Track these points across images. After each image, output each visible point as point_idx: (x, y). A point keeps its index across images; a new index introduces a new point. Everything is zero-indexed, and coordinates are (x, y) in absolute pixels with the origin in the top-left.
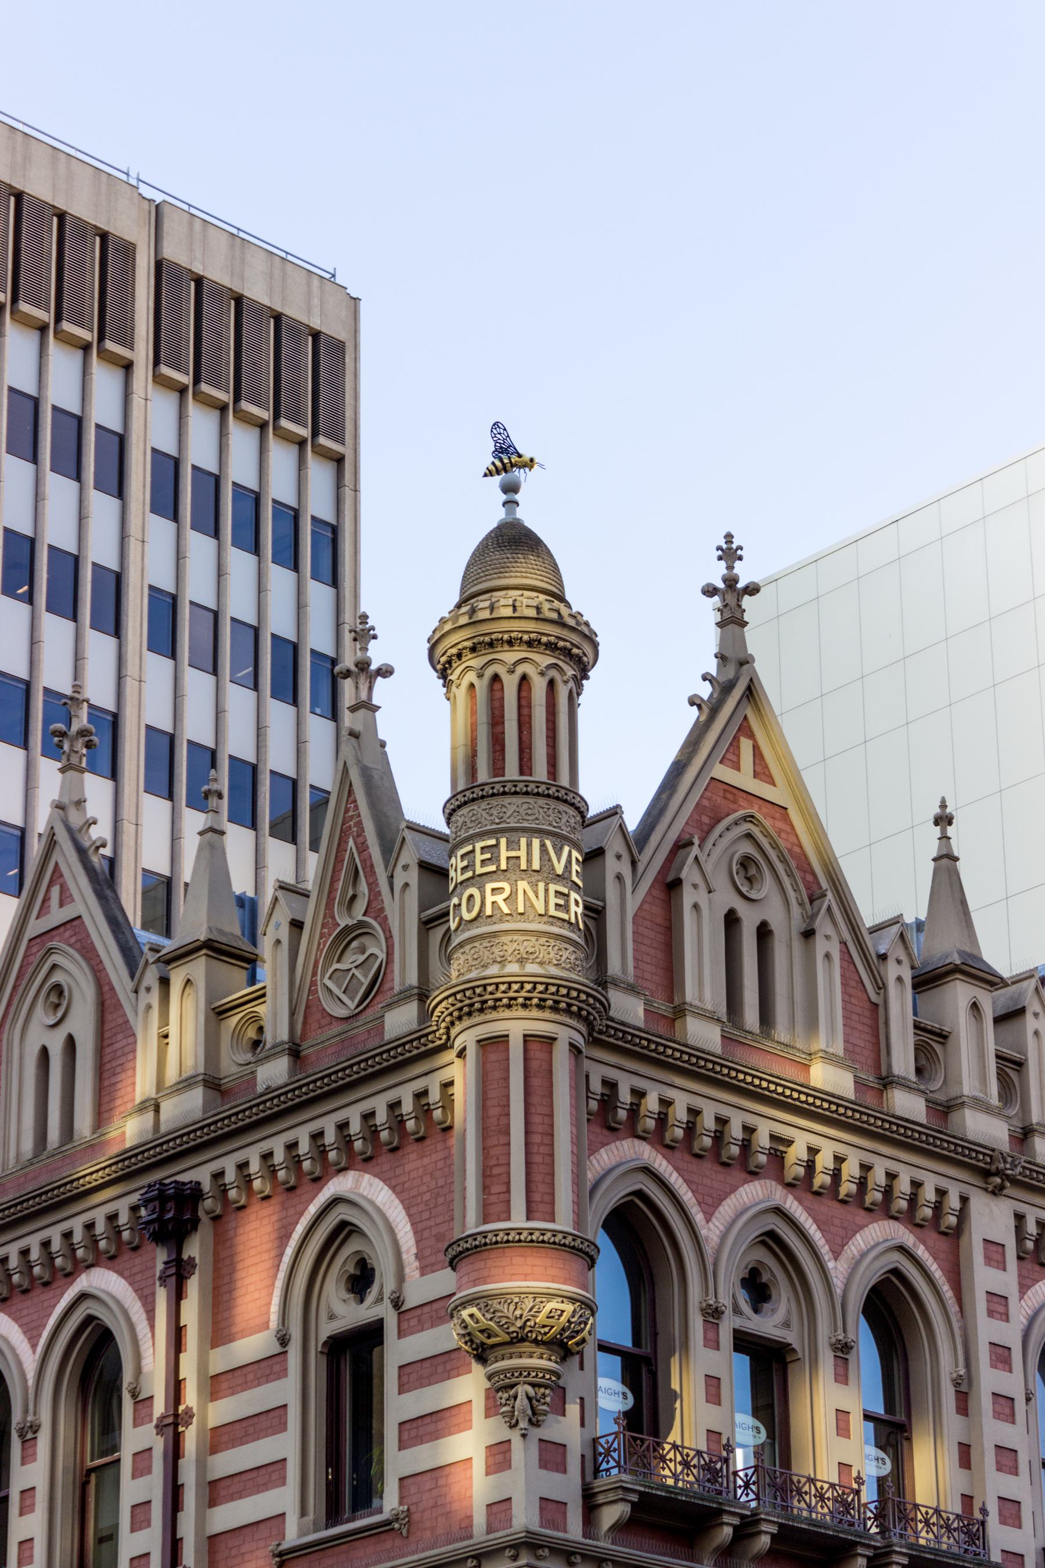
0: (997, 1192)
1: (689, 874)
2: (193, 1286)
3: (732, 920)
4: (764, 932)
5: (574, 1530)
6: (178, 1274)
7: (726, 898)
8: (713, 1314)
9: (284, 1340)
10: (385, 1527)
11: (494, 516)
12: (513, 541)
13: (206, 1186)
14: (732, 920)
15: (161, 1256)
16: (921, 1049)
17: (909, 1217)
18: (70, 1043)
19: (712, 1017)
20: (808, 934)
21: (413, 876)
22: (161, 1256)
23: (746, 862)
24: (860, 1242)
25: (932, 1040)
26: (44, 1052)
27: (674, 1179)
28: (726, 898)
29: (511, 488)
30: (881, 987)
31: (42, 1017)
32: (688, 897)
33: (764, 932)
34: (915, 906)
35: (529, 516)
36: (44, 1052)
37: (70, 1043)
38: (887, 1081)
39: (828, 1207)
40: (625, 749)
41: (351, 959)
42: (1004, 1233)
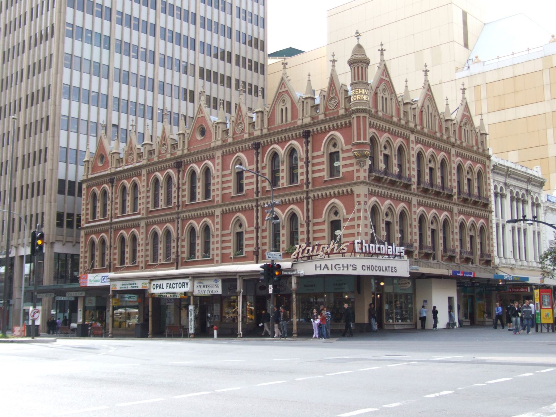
0: (413, 133)
1: (378, 92)
2: (310, 144)
3: (382, 97)
4: (386, 99)
5: (367, 180)
6: (307, 143)
7: (382, 95)
8: (381, 151)
9: (324, 153)
10: (340, 178)
11: (357, 43)
12: (359, 46)
13: (311, 131)
14: (382, 97)
15: (304, 140)
16: (404, 114)
17: (403, 138)
18: (286, 108)
19: (412, 123)
20: (391, 99)
21: (343, 91)
22: (304, 140)
23: (384, 89)
24: (397, 141)
25: (406, 113)
26: (282, 109)
27: (377, 133)
28: (382, 95)
29: (358, 39)
30: (399, 106)
31: (281, 104)
32: (378, 95)
33: (386, 99)
34: (444, 111)
35: (361, 43)
36: (282, 109)
37: (286, 108)
38: (400, 119)
39: (426, 147)
40: (372, 74)
41: (333, 101)
42: (414, 140)
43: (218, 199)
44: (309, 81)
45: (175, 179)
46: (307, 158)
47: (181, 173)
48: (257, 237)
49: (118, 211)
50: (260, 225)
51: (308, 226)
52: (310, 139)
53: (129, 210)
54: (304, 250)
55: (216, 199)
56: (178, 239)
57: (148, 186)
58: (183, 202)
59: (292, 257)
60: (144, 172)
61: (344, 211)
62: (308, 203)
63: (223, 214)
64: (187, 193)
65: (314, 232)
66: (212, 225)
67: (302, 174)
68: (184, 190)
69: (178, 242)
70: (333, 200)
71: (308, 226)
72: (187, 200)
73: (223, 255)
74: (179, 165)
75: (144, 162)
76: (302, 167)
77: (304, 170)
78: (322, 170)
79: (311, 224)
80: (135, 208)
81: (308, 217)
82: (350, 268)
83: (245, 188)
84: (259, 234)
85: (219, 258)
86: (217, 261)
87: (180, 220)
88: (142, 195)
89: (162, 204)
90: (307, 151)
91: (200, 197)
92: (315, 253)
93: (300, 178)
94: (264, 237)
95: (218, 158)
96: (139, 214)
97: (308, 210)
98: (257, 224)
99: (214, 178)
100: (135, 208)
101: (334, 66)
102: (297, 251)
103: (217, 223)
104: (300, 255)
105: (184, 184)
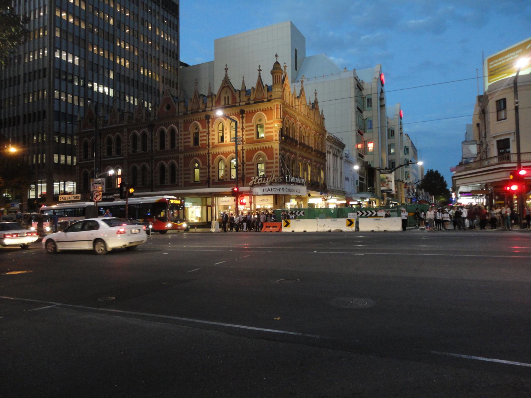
6: (243, 118)
43: (182, 149)
44: (243, 81)
45: (148, 134)
46: (243, 126)
47: (154, 132)
48: (209, 172)
49: (105, 154)
50: (211, 164)
51: (243, 166)
52: (244, 115)
53: (114, 153)
54: (257, 181)
55: (180, 149)
56: (152, 172)
57: (128, 139)
58: (213, 143)
59: (250, 184)
60: (125, 130)
61: (267, 158)
62: (152, 162)
63: (185, 157)
64: (158, 144)
65: (247, 169)
66: (177, 164)
67: (149, 147)
68: (156, 142)
69: (152, 174)
70: (195, 158)
71: (243, 166)
72: (158, 148)
73: (185, 182)
74: (151, 127)
75: (125, 123)
76: (149, 143)
77: (150, 145)
78: (253, 134)
79: (245, 165)
80: (118, 152)
81: (243, 161)
82: (281, 190)
83: (200, 143)
84: (245, 167)
85: (183, 184)
86: (181, 186)
87: (153, 161)
88: (124, 144)
89: (139, 150)
90: (243, 123)
91: (168, 146)
92: (264, 182)
93: (148, 149)
94: (156, 177)
95: (181, 123)
96: (122, 156)
97: (152, 166)
98: (209, 164)
99: (123, 143)
100: (118, 152)
101: (260, 73)
102: (253, 181)
103: (181, 163)
104: (255, 183)
105: (156, 139)
